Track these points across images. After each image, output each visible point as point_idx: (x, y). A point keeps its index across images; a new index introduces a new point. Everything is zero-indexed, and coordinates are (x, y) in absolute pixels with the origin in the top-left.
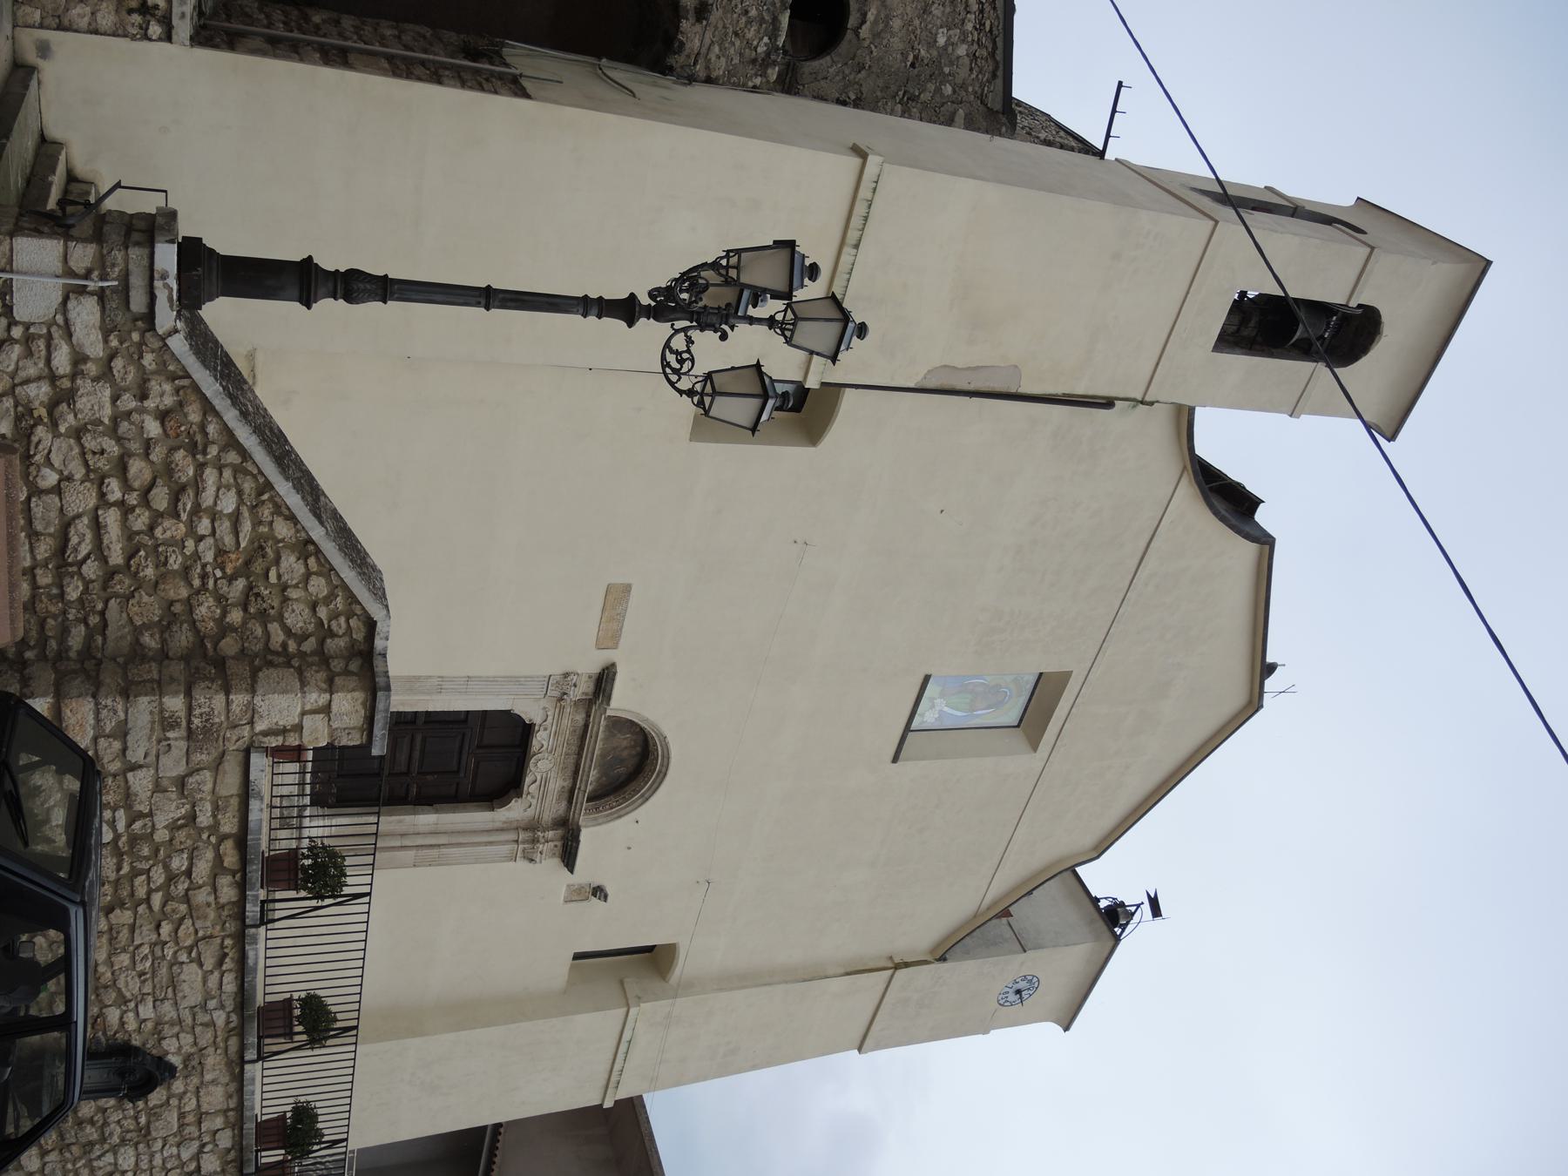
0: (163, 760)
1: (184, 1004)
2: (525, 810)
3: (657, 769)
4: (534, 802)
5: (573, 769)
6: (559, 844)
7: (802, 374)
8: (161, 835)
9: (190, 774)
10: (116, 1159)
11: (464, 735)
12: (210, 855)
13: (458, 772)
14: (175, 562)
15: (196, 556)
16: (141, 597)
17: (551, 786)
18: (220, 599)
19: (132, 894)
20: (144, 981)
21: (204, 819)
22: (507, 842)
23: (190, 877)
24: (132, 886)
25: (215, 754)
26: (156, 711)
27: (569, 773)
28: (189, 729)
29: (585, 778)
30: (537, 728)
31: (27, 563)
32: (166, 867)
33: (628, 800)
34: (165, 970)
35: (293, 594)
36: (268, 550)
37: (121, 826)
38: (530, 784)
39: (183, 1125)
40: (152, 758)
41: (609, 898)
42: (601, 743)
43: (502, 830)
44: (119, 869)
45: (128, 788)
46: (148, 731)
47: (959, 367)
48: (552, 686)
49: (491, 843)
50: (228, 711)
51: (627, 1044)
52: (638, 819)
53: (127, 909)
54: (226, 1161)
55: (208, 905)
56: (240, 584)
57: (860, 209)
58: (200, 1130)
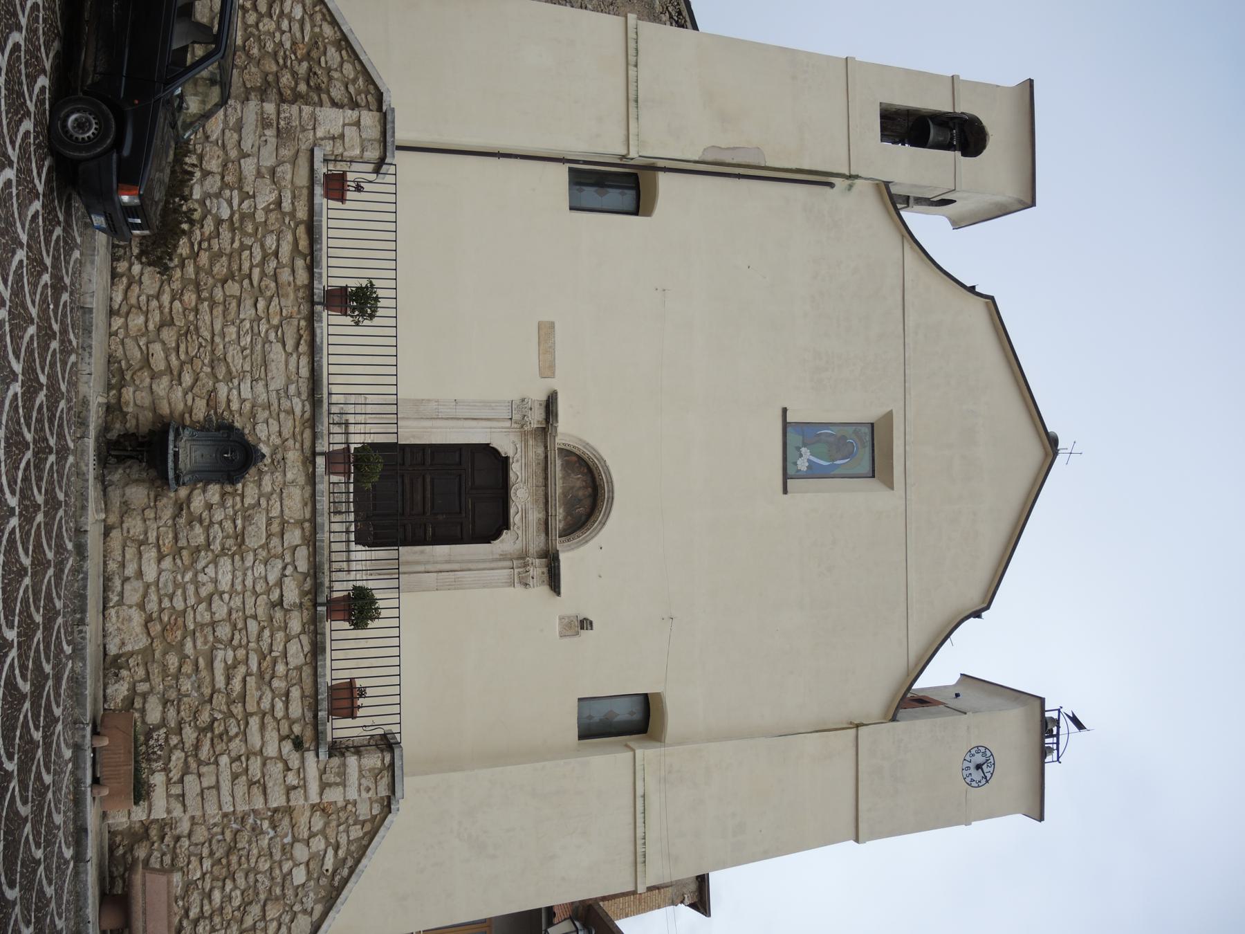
0: (263, 150)
1: (272, 387)
2: (515, 543)
4: (520, 533)
6: (545, 570)
7: (626, 148)
8: (260, 217)
9: (278, 165)
10: (216, 573)
12: (290, 237)
13: (460, 513)
14: (270, 47)
15: (281, 44)
16: (250, 68)
18: (294, 74)
19: (240, 269)
20: (244, 358)
21: (286, 206)
23: (277, 257)
24: (240, 260)
25: (293, 152)
26: (259, 112)
27: (542, 505)
28: (278, 128)
31: (192, 627)
32: (262, 246)
34: (260, 346)
35: (336, 75)
36: (320, 43)
37: (235, 202)
38: (515, 518)
39: (270, 536)
40: (255, 149)
41: (594, 625)
42: (561, 481)
43: (500, 560)
44: (233, 242)
45: (241, 172)
46: (254, 127)
47: (723, 147)
49: (492, 569)
50: (300, 117)
51: (642, 799)
52: (602, 546)
53: (236, 281)
54: (303, 591)
55: (289, 284)
56: (305, 65)
57: (632, 44)
58: (283, 546)
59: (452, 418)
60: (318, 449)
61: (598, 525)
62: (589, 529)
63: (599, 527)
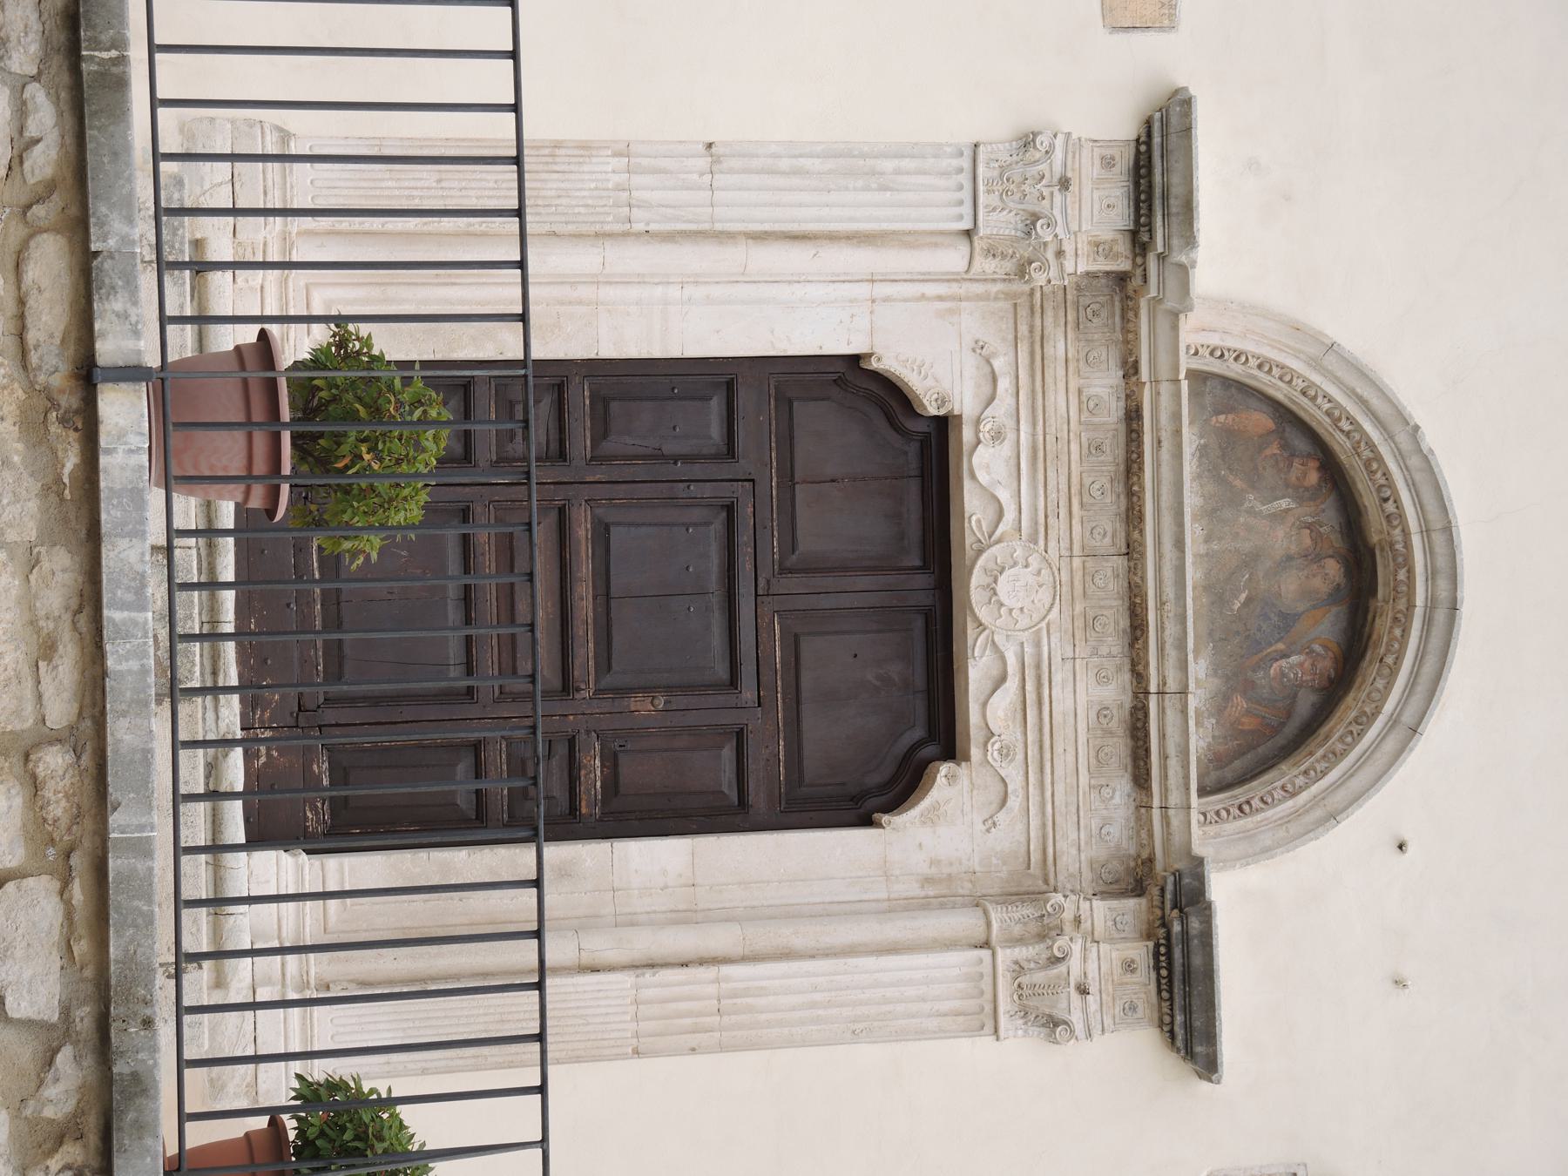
2: (990, 823)
3: (1420, 600)
4: (1016, 783)
5: (1124, 623)
11: (730, 509)
17: (1062, 699)
22: (950, 945)
27: (1114, 644)
29: (1171, 630)
30: (967, 434)
33: (1344, 754)
48: (994, 200)
60: (109, 350)
62: (1338, 756)
63: (1390, 745)
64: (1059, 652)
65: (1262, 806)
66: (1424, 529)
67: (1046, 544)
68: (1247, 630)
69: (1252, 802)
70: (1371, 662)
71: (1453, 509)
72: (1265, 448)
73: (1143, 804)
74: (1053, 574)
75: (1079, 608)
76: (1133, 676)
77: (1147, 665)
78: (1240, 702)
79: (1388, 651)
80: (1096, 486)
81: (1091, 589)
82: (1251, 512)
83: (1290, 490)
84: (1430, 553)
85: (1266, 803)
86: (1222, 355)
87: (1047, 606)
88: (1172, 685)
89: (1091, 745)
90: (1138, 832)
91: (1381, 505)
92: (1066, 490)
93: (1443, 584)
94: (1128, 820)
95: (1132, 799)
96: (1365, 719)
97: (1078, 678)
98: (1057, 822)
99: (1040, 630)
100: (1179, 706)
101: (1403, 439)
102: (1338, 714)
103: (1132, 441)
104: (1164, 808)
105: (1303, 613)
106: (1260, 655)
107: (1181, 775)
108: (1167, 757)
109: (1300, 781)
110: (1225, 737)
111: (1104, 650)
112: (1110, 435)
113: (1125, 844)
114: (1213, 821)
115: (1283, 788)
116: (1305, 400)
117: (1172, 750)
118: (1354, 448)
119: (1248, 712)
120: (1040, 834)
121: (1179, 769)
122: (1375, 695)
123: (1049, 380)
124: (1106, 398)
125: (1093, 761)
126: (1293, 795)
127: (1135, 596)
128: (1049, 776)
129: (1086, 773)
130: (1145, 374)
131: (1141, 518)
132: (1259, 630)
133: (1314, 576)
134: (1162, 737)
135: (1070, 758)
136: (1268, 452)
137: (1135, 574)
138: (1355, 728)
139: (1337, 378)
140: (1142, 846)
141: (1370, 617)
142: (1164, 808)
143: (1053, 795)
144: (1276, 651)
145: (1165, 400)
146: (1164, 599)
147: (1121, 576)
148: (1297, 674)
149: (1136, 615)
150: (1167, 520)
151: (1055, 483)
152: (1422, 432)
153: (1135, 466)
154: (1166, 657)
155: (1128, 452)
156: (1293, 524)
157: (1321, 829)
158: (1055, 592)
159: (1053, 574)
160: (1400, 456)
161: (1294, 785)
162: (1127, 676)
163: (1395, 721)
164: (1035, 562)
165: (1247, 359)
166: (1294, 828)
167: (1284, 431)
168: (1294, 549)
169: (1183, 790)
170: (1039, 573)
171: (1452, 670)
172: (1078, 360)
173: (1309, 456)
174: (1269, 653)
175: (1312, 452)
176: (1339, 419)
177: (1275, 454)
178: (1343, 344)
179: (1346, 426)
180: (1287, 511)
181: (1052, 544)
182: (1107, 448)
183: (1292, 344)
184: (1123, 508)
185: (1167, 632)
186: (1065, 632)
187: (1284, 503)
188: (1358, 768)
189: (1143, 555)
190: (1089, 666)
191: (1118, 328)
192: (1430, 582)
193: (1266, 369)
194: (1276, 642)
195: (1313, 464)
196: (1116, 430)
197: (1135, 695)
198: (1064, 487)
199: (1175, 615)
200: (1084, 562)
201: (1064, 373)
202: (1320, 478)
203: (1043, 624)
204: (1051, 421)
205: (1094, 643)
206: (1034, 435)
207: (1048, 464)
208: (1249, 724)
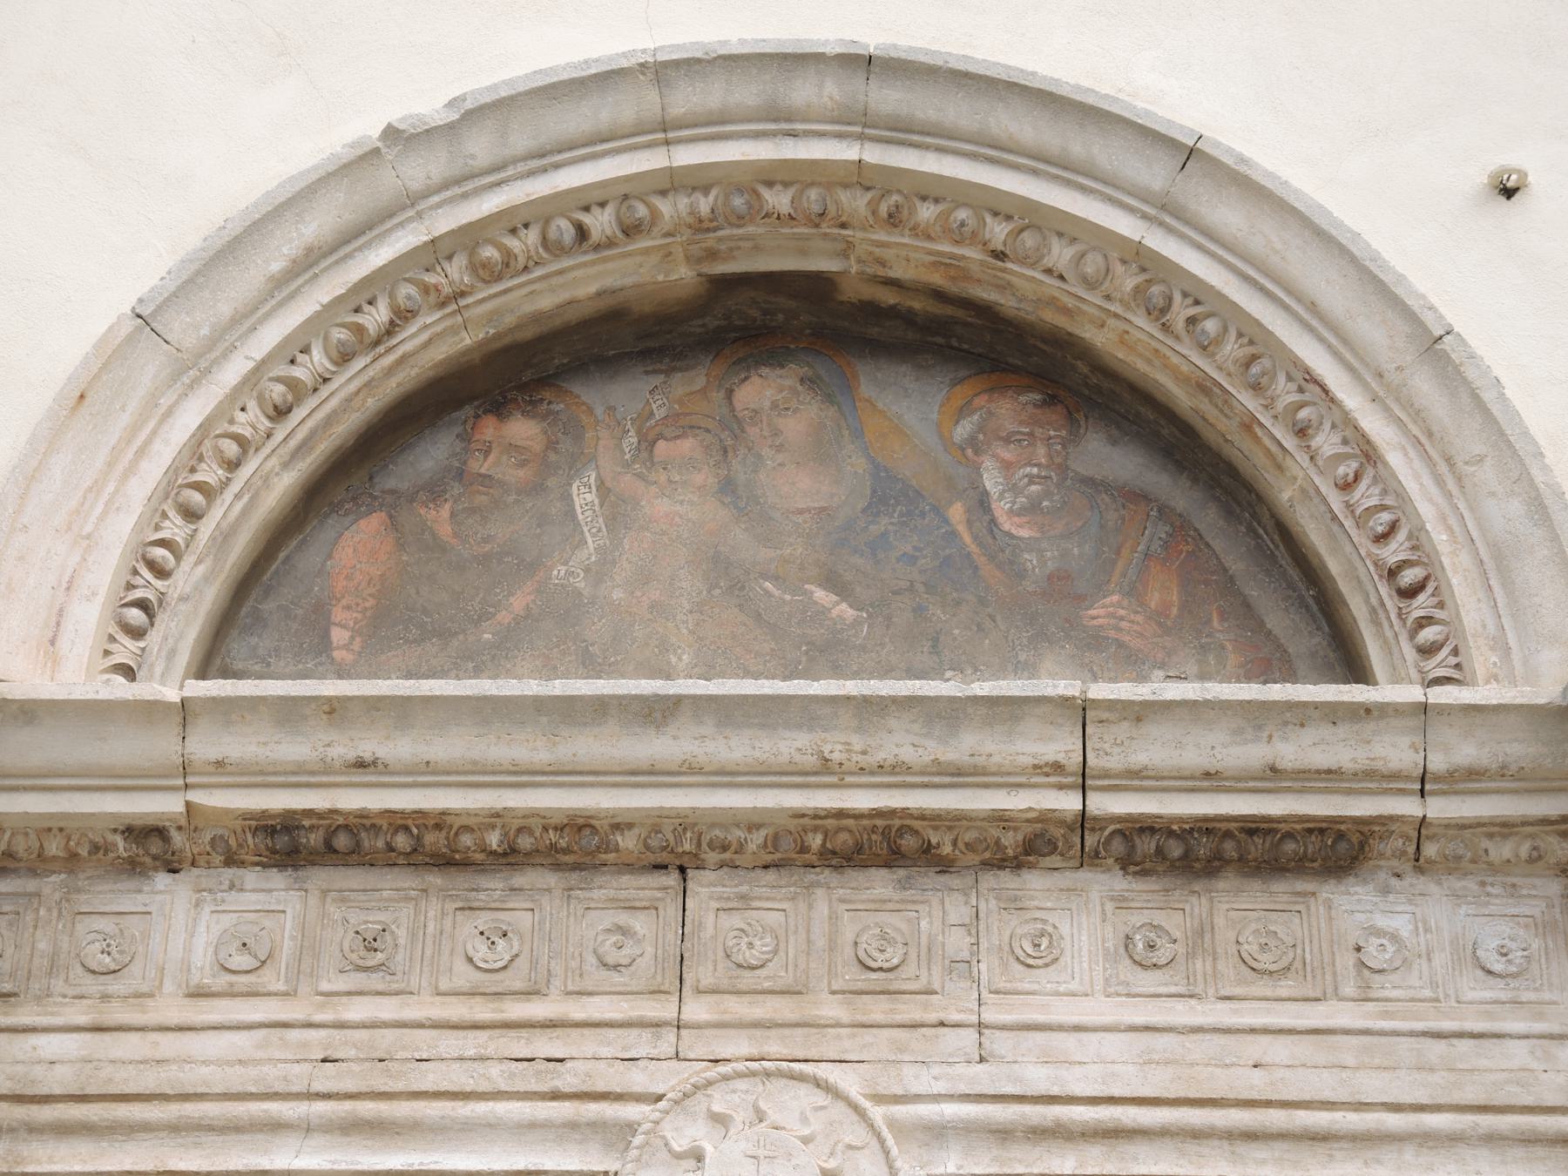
3: (847, 152)
5: (880, 884)
52: (1478, 176)
59: (872, 1026)
61: (1208, 238)
62: (1257, 342)
63: (1228, 216)
64: (960, 1069)
65: (1401, 535)
66: (661, 136)
67: (639, 1098)
68: (911, 588)
69: (1392, 560)
70: (1005, 287)
71: (610, 58)
72: (434, 536)
73: (1411, 849)
74: (726, 1078)
75: (832, 1009)
76: (1032, 866)
77: (1001, 819)
78: (1106, 610)
79: (975, 238)
80: (480, 951)
81: (776, 974)
82: (598, 572)
83: (551, 482)
84: (723, 123)
85: (1393, 527)
86: (143, 605)
87: (821, 1099)
88: (1062, 746)
89: (1238, 991)
90: (1494, 869)
91: (597, 247)
92: (483, 1036)
93: (804, 92)
94: (1457, 896)
95: (1394, 881)
96: (1155, 290)
97: (1040, 1018)
98: (1481, 1099)
99: (892, 1123)
100: (1123, 730)
101: (419, 170)
102: (1142, 366)
103: (356, 849)
104: (1424, 784)
105: (872, 460)
106: (981, 560)
107: (1326, 731)
108: (1273, 769)
109: (1327, 442)
110: (1204, 649)
111: (957, 943)
112: (336, 913)
113: (1535, 908)
114: (1453, 660)
115: (1346, 486)
116: (298, 414)
117: (1251, 754)
118: (443, 305)
119: (1134, 592)
120: (1519, 1152)
121: (1309, 735)
122: (1092, 265)
123: (149, 1081)
124: (227, 920)
125: (1285, 988)
126: (1369, 454)
127: (804, 849)
128: (1338, 1115)
129: (1321, 1008)
130: (164, 805)
131: (579, 824)
132: (912, 560)
133: (776, 433)
134: (1211, 780)
135: (1278, 1050)
136: (445, 530)
137: (740, 850)
138: (1181, 312)
139: (235, 321)
140: (1535, 858)
141: (889, 298)
142: (1424, 784)
143: (1397, 1108)
144: (969, 523)
145: (241, 745)
146: (810, 761)
147: (744, 889)
148: (1032, 479)
149: (859, 849)
150: (587, 746)
151: (456, 1065)
152: (404, 119)
153: (430, 838)
154: (980, 761)
155: (390, 859)
156: (639, 476)
157: (1470, 373)
158: (781, 1074)
159: (726, 1078)
160: (462, 183)
161: (1339, 458)
162: (1035, 883)
163: (1163, 208)
164: (685, 1132)
165: (162, 543)
166: (1469, 441)
167: (393, 492)
168: (704, 477)
169: (1370, 726)
170: (720, 1120)
171: (1030, 67)
172: (105, 997)
173: (465, 438)
174: (975, 538)
175: (458, 429)
176: (359, 330)
177: (453, 515)
178: (142, 289)
179: (376, 317)
180: (603, 490)
181: (637, 1079)
182: (372, 921)
183: (125, 419)
184: (551, 879)
185: (907, 754)
186: (901, 1049)
187: (584, 496)
188: (1289, 292)
189: (685, 822)
190: (1001, 985)
191: (31, 885)
192: (799, 126)
193: (197, 498)
194: (946, 521)
195: (489, 429)
196: (325, 893)
197: (1088, 859)
198: (471, 1043)
199: (859, 729)
200: (699, 991)
201: (134, 1037)
202: (525, 413)
203: (877, 1113)
204: (272, 1076)
205: (936, 971)
206: (308, 1128)
207: (399, 1086)
208: (1164, 591)
